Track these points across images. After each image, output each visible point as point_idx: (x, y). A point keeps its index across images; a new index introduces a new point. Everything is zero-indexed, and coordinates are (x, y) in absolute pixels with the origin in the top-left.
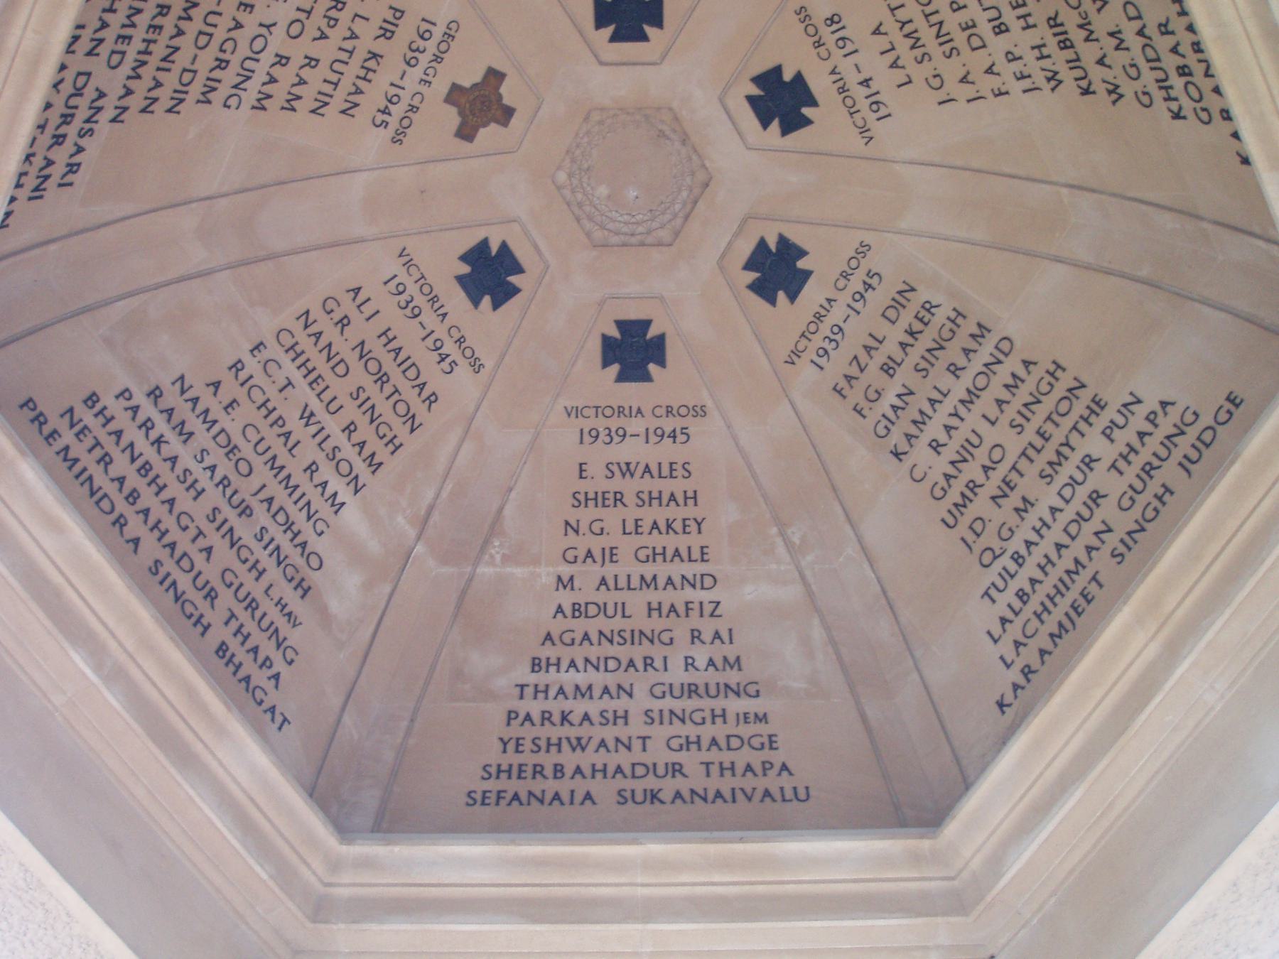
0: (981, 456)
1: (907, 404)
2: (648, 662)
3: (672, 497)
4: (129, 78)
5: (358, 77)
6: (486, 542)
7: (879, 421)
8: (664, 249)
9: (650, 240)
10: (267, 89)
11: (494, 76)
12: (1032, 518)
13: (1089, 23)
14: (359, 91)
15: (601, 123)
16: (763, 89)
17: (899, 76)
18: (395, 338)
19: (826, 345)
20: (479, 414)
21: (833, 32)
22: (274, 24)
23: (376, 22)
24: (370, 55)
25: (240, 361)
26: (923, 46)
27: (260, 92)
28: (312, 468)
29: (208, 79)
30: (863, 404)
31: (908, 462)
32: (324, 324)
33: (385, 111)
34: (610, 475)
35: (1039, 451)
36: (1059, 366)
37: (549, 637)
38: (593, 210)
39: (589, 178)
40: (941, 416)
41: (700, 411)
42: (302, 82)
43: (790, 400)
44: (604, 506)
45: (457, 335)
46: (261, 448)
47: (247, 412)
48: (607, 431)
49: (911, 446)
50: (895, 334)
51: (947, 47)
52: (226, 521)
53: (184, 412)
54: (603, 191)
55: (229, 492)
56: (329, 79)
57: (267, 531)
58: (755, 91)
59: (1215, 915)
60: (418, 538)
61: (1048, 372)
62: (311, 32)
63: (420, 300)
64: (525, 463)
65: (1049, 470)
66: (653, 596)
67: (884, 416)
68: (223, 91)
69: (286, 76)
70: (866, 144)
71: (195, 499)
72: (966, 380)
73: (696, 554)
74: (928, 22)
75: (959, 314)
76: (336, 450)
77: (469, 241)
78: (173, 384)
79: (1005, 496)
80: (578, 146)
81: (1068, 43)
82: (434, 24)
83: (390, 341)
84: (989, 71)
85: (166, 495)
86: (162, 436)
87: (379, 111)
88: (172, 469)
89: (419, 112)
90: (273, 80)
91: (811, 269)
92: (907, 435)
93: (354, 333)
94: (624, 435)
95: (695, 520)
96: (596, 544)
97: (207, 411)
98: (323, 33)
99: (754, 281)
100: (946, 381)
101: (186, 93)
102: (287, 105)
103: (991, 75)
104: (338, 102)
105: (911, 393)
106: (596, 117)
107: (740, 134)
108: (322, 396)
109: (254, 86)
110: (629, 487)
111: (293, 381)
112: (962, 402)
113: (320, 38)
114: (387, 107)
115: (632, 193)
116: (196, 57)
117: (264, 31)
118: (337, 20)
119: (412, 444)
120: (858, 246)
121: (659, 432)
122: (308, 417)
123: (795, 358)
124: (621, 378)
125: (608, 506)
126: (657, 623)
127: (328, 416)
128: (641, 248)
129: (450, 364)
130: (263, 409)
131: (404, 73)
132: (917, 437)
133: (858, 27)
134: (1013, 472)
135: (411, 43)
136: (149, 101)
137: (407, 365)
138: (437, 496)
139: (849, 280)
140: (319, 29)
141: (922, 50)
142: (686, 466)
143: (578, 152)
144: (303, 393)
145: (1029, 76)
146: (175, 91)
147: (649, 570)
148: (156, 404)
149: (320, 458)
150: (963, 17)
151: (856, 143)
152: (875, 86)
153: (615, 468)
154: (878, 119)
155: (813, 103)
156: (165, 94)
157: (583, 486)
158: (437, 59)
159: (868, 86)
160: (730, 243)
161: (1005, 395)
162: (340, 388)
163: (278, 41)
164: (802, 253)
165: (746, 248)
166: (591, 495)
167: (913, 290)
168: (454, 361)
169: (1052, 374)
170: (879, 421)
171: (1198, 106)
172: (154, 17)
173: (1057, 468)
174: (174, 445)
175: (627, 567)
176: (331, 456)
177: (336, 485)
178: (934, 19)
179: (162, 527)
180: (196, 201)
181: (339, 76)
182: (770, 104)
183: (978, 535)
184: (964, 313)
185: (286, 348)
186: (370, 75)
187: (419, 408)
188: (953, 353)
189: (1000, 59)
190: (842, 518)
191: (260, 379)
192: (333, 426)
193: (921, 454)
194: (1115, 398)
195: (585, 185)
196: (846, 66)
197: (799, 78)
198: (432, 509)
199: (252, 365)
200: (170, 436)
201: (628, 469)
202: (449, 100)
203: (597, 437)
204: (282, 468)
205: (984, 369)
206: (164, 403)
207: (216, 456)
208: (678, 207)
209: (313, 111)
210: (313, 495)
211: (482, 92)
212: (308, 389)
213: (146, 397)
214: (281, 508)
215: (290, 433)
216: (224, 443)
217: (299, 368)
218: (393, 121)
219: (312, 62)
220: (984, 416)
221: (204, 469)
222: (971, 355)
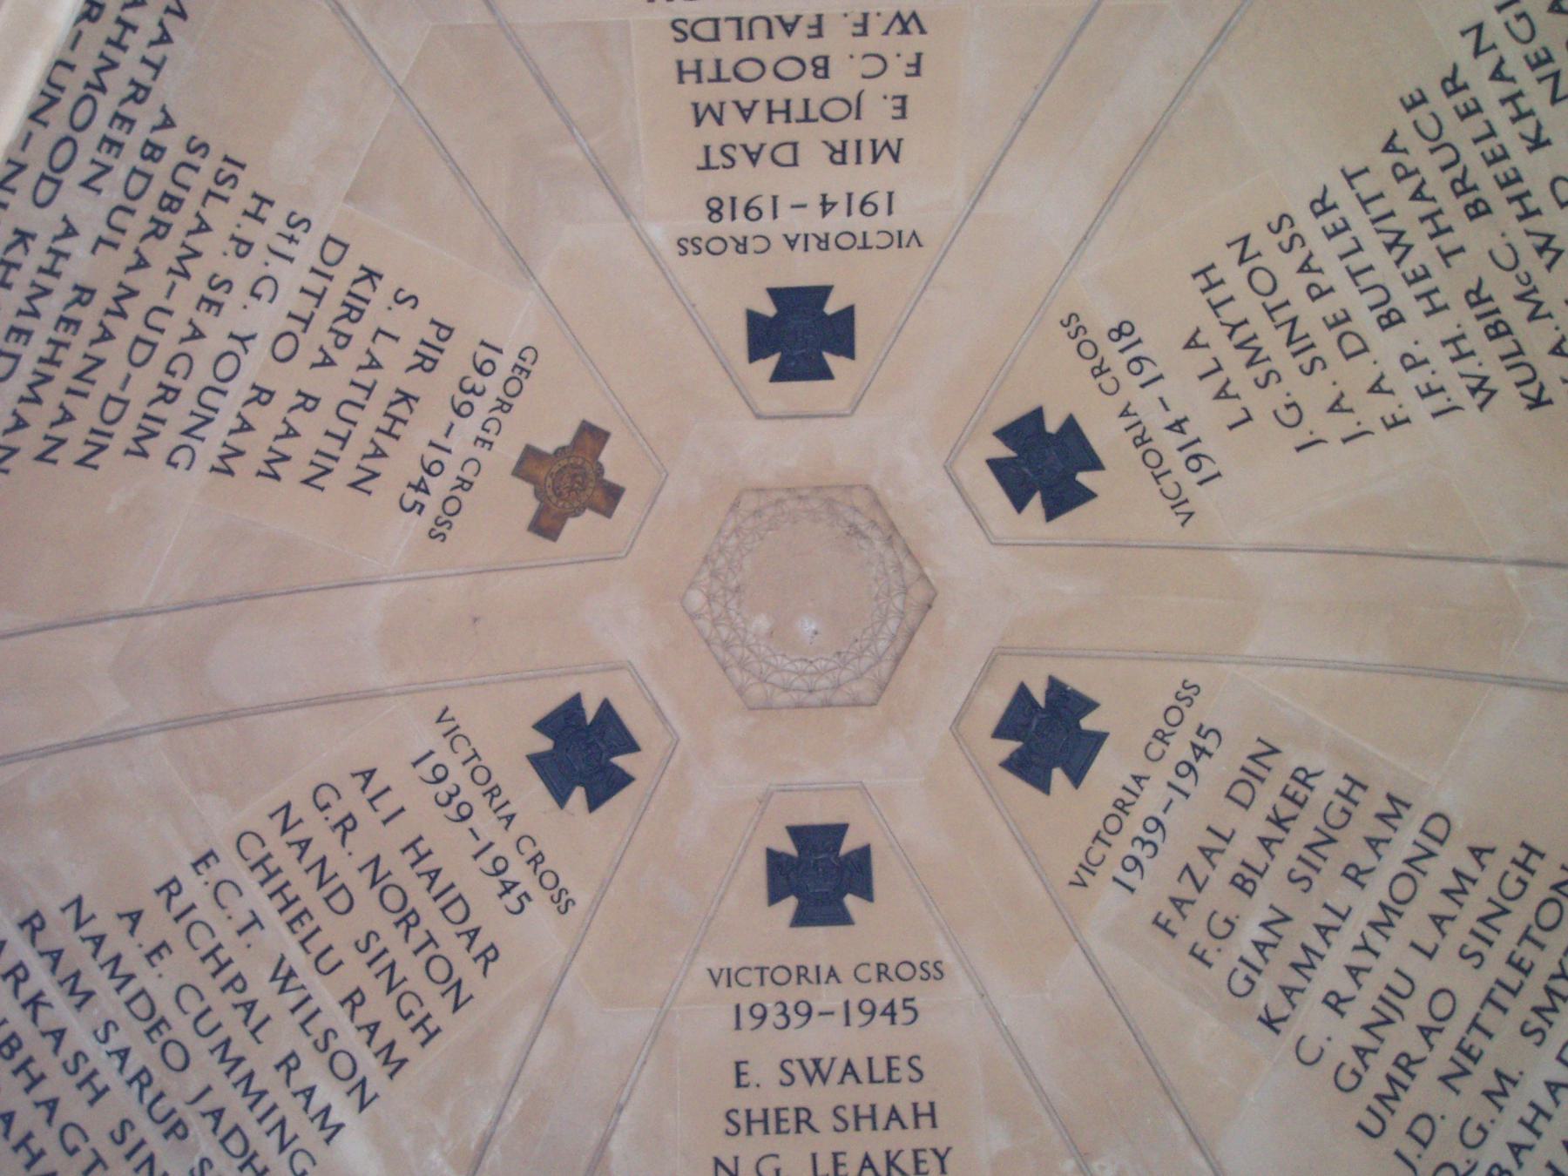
0: (1416, 1010)
1: (1280, 937)
3: (894, 1114)
4: (22, 400)
5: (379, 430)
7: (1235, 970)
8: (864, 711)
9: (839, 697)
10: (236, 440)
11: (591, 436)
12: (1517, 1105)
13: (1535, 290)
14: (380, 454)
15: (757, 513)
18: (430, 853)
19: (1137, 850)
20: (567, 981)
22: (253, 337)
23: (409, 344)
24: (399, 396)
25: (174, 880)
26: (1268, 359)
27: (225, 445)
28: (289, 1064)
29: (146, 416)
30: (1205, 942)
31: (1290, 1033)
32: (315, 827)
33: (420, 487)
34: (787, 1079)
35: (1514, 993)
36: (1532, 851)
38: (747, 653)
39: (739, 604)
40: (1341, 951)
41: (933, 971)
42: (291, 433)
43: (1080, 945)
44: (779, 1131)
46: (204, 1026)
47: (182, 965)
48: (780, 1008)
49: (1294, 1006)
50: (1253, 824)
51: (1305, 359)
52: (142, 1143)
53: (78, 954)
54: (762, 623)
55: (149, 1095)
56: (333, 430)
57: (211, 1166)
58: (1002, 451)
61: (1514, 861)
63: (471, 793)
64: (645, 1063)
65: (1536, 1022)
67: (1242, 960)
68: (169, 437)
69: (267, 420)
70: (1072, 883)
71: (92, 1102)
72: (1378, 889)
74: (1273, 320)
75: (1355, 783)
76: (331, 1035)
77: (552, 698)
78: (64, 910)
79: (1465, 1072)
80: (720, 551)
81: (1502, 328)
82: (499, 351)
83: (421, 858)
84: (1376, 388)
85: (42, 1092)
86: (41, 994)
87: (410, 485)
88: (56, 1050)
89: (473, 489)
90: (246, 427)
91: (1104, 730)
92: (1283, 989)
93: (362, 844)
94: (809, 1014)
95: (935, 1151)
97: (117, 959)
98: (326, 356)
99: (1012, 755)
100: (1344, 894)
101: (110, 435)
102: (265, 469)
103: (1378, 395)
104: (346, 470)
105: (1286, 919)
106: (750, 503)
107: (980, 521)
108: (307, 944)
109: (216, 434)
110: (820, 1099)
111: (261, 917)
112: (1374, 925)
113: (323, 364)
116: (129, 377)
117: (236, 346)
118: (349, 337)
119: (456, 1029)
120: (1179, 687)
121: (867, 1007)
122: (284, 977)
123: (1086, 876)
124: (800, 920)
125: (787, 1132)
127: (317, 978)
128: (826, 709)
129: (519, 899)
130: (211, 961)
132: (1302, 991)
133: (1159, 340)
134: (1474, 1031)
135: (464, 378)
136: (50, 443)
137: (449, 898)
138: (499, 1118)
139: (1168, 744)
140: (321, 349)
141: (1266, 366)
142: (915, 1062)
143: (721, 561)
144: (278, 937)
145: (1442, 389)
146: (93, 431)
148: (33, 941)
149: (304, 1047)
150: (1328, 306)
151: (1167, 523)
152: (1192, 430)
153: (795, 1069)
154: (1201, 483)
155: (1095, 464)
156: (75, 434)
157: (743, 1100)
158: (504, 406)
161: (1446, 907)
162: (338, 932)
163: (255, 367)
164: (1089, 706)
165: (996, 703)
166: (757, 1115)
167: (1275, 751)
168: (525, 894)
169: (1523, 866)
170: (1235, 970)
172: (68, 305)
173: (1550, 1016)
174: (60, 1010)
176: (321, 1045)
177: (329, 1093)
178: (1281, 316)
179: (35, 1145)
180: (114, 618)
181: (350, 426)
182: (1026, 470)
183: (1425, 1145)
184: (1363, 782)
185: (252, 862)
187: (467, 969)
188: (1351, 847)
189: (1393, 367)
190: (1183, 1137)
191: (206, 911)
192: (326, 995)
193: (1312, 1018)
195: (733, 613)
196: (1145, 402)
197: (1071, 425)
198: (488, 1143)
199: (195, 889)
200: (53, 994)
201: (818, 1070)
202: (520, 471)
203: (764, 1017)
204: (239, 1060)
205: (1406, 868)
206: (47, 941)
207: (129, 1034)
208: (882, 645)
209: (306, 482)
210: (290, 1108)
211: (572, 461)
212: (285, 931)
213: (18, 928)
214: (236, 1128)
215: (254, 1003)
216: (144, 1013)
217: (271, 896)
218: (432, 503)
219: (308, 401)
220: (1413, 945)
221: (109, 1054)
222: (1382, 848)
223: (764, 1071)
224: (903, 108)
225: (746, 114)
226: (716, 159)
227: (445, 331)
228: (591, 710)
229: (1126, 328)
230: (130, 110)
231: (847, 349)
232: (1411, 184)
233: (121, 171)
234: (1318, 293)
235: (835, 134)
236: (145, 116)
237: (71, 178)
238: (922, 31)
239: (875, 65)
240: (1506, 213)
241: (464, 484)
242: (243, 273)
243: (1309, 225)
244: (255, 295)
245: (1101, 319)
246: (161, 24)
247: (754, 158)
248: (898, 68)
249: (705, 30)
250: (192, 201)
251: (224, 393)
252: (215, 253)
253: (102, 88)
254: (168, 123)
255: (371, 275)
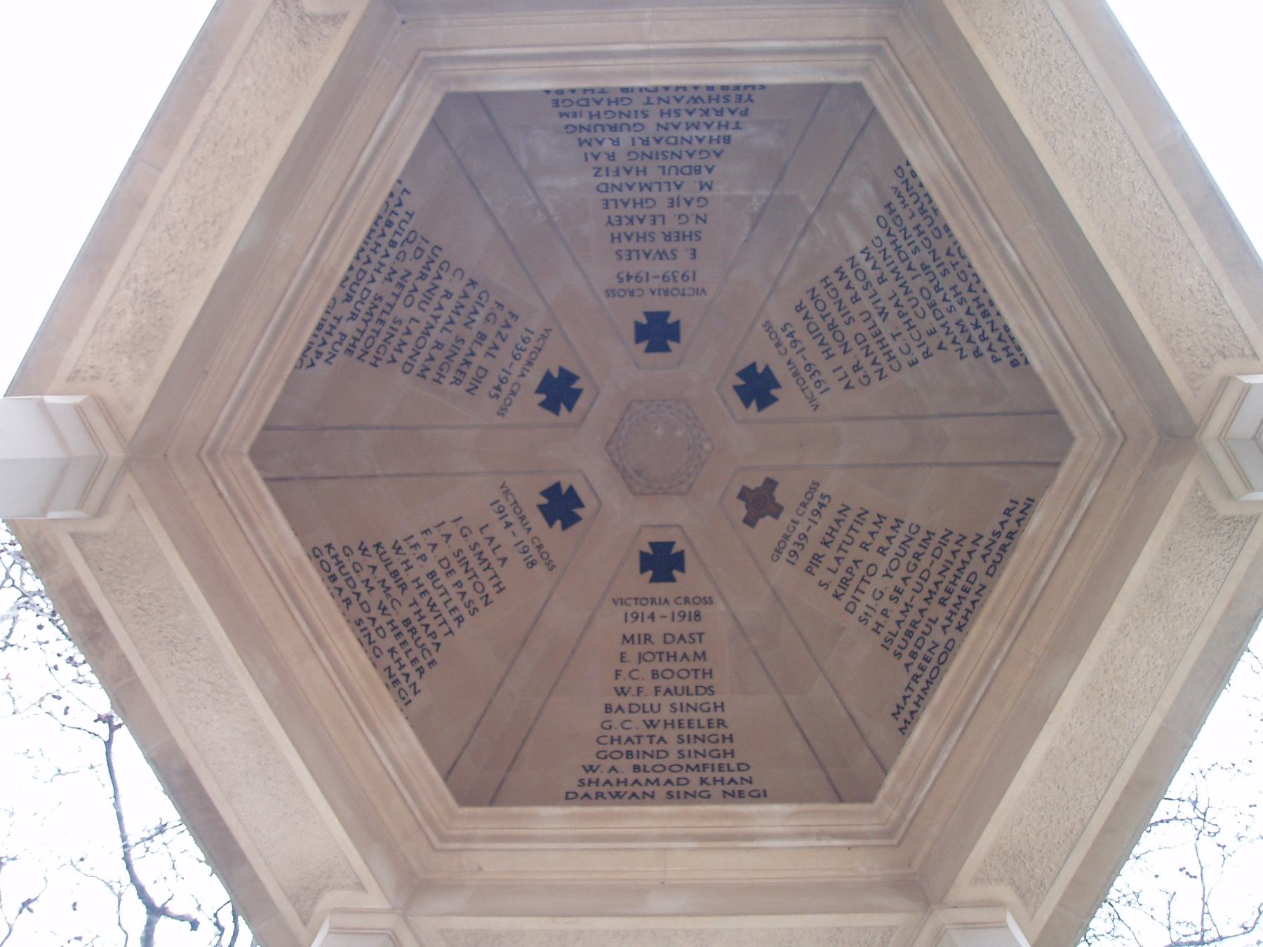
0: (418, 297)
2: (646, 142)
3: (629, 238)
6: (764, 208)
10: (893, 533)
11: (750, 521)
14: (837, 521)
15: (681, 483)
16: (573, 513)
17: (488, 532)
21: (531, 556)
22: (884, 576)
28: (882, 280)
30: (497, 311)
31: (466, 280)
32: (870, 370)
37: (718, 155)
40: (445, 315)
41: (610, 293)
42: (872, 534)
44: (678, 233)
45: (781, 348)
50: (478, 360)
54: (679, 433)
58: (578, 511)
59: (277, 119)
60: (811, 217)
62: (863, 566)
63: (806, 375)
66: (642, 179)
72: (431, 341)
73: (612, 204)
77: (771, 411)
84: (434, 546)
90: (889, 538)
96: (684, 209)
104: (851, 516)
109: (901, 537)
110: (660, 244)
112: (432, 327)
114: (821, 508)
115: (659, 432)
117: (890, 573)
122: (883, 313)
124: (666, 314)
126: (640, 164)
127: (870, 310)
131: (808, 530)
133: (516, 560)
137: (815, 333)
138: (797, 242)
144: (886, 330)
147: (646, 194)
149: (875, 285)
150: (454, 579)
153: (670, 256)
156: (951, 546)
157: (694, 244)
158: (786, 537)
159: (506, 523)
160: (592, 403)
162: (860, 326)
163: (883, 563)
165: (581, 403)
166: (687, 239)
171: (321, 558)
174: (968, 321)
175: (662, 196)
178: (471, 574)
186: (829, 531)
187: (809, 304)
188: (440, 356)
189: (430, 556)
191: (914, 345)
192: (866, 303)
193: (457, 287)
194: (341, 357)
196: (522, 535)
212: (882, 330)
217: (887, 345)
218: (817, 498)
219: (864, 546)
223: (683, 255)
224: (622, 657)
225: (685, 656)
226: (697, 637)
227: (809, 570)
228: (754, 405)
229: (530, 565)
230: (919, 672)
231: (643, 555)
232: (430, 631)
233: (925, 648)
234: (458, 584)
235: (649, 647)
236: (914, 669)
237: (940, 649)
238: (615, 688)
239: (634, 675)
240: (398, 623)
241: (804, 505)
242: (885, 603)
243: (463, 611)
244: (881, 592)
245: (540, 569)
246: (905, 703)
247: (682, 637)
248: (624, 674)
249: (701, 691)
250: (901, 633)
251: (896, 554)
252: (895, 610)
253: (927, 682)
254: (907, 665)
255: (837, 596)
